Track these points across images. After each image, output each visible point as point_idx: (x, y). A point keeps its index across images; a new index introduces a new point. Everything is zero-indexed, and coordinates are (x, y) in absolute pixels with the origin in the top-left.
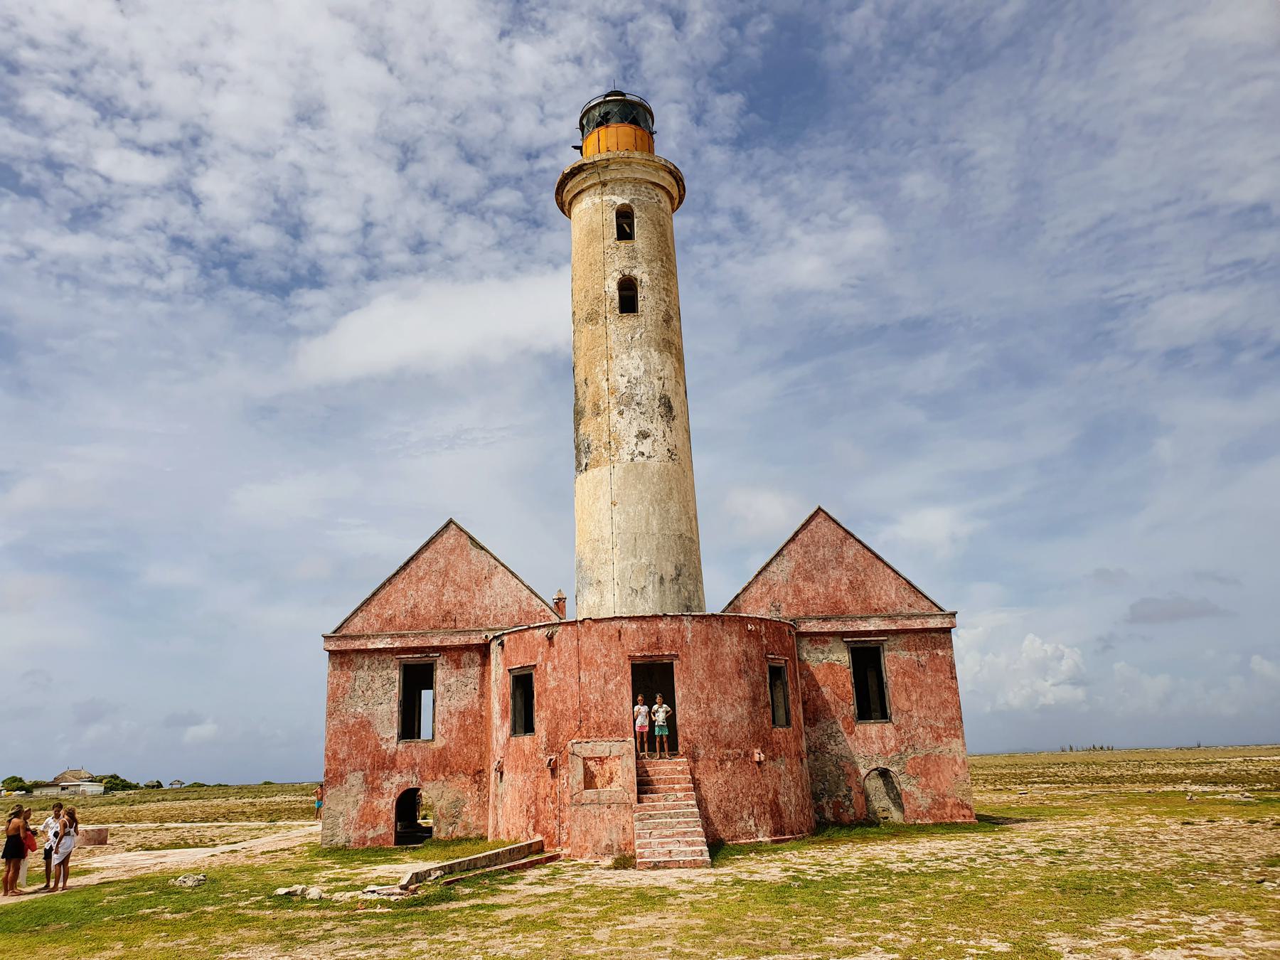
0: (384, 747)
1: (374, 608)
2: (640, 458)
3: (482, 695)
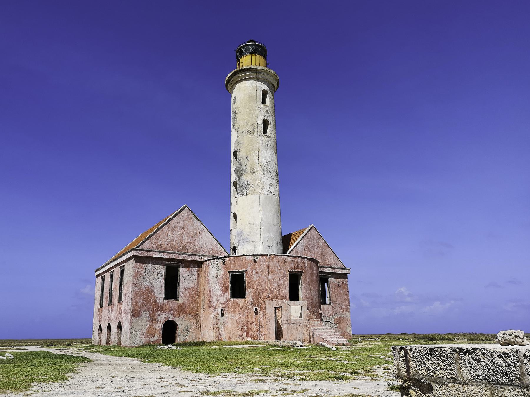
0: (158, 301)
1: (154, 239)
2: (270, 194)
3: (198, 283)
